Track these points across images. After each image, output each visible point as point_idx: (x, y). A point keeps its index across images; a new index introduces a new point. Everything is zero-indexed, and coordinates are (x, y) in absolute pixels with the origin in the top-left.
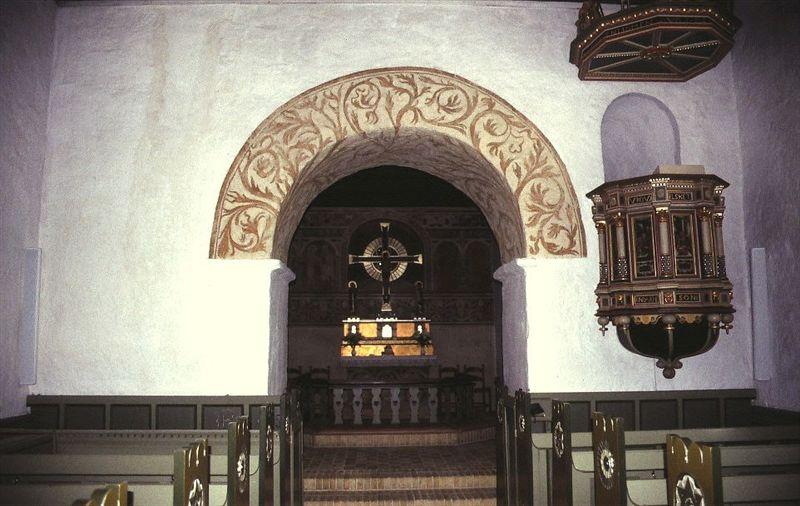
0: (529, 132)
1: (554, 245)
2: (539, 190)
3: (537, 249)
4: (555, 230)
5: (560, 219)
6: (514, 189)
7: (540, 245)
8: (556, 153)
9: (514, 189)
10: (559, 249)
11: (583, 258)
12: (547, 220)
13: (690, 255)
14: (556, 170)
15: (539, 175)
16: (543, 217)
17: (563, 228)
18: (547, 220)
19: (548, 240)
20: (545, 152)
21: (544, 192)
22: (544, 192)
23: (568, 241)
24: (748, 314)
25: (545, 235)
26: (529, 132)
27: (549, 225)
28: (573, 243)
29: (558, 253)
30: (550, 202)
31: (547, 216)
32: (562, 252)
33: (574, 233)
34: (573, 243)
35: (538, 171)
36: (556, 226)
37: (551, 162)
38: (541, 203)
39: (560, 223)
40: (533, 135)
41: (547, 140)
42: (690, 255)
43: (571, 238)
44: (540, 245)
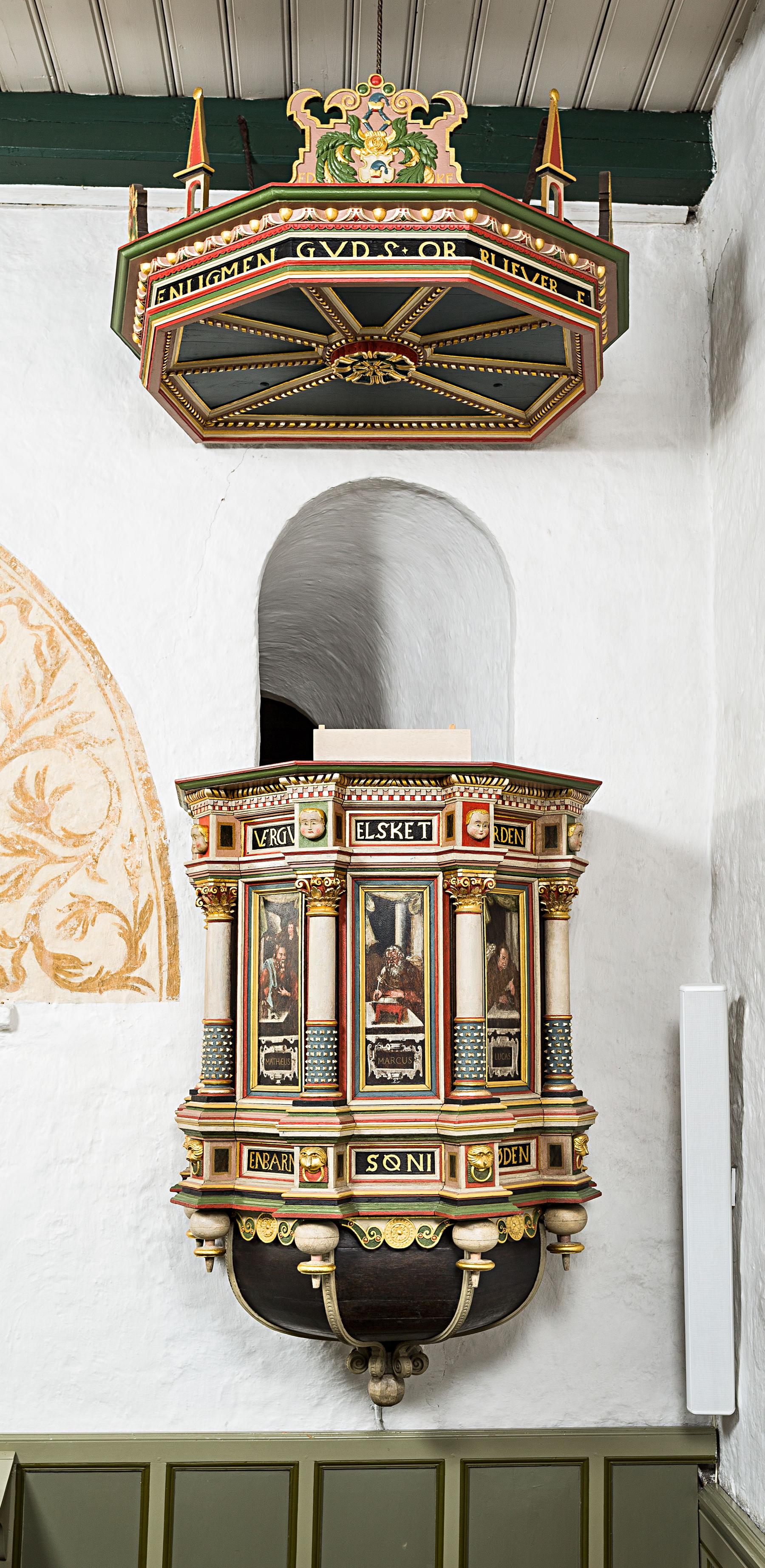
0: (24, 607)
1: (75, 962)
2: (41, 794)
3: (20, 973)
4: (81, 915)
5: (98, 879)
6: (594, 230)
7: (29, 959)
8: (107, 675)
9: (594, 230)
10: (89, 972)
11: (167, 1004)
12: (59, 881)
13: (413, 1021)
14: (101, 725)
15: (44, 742)
16: (47, 873)
17: (107, 907)
18: (59, 881)
19: (56, 945)
20: (75, 669)
21: (59, 792)
22: (59, 792)
23: (121, 948)
24: (420, 1061)
25: (47, 928)
26: (24, 607)
27: (61, 898)
28: (135, 954)
29: (83, 987)
30: (75, 826)
31: (61, 869)
32: (101, 983)
33: (143, 921)
34: (135, 954)
35: (44, 728)
36: (86, 901)
37: (88, 698)
38: (42, 823)
39: (99, 893)
40: (34, 617)
41: (79, 631)
42: (413, 1021)
43: (132, 940)
44: (29, 959)
